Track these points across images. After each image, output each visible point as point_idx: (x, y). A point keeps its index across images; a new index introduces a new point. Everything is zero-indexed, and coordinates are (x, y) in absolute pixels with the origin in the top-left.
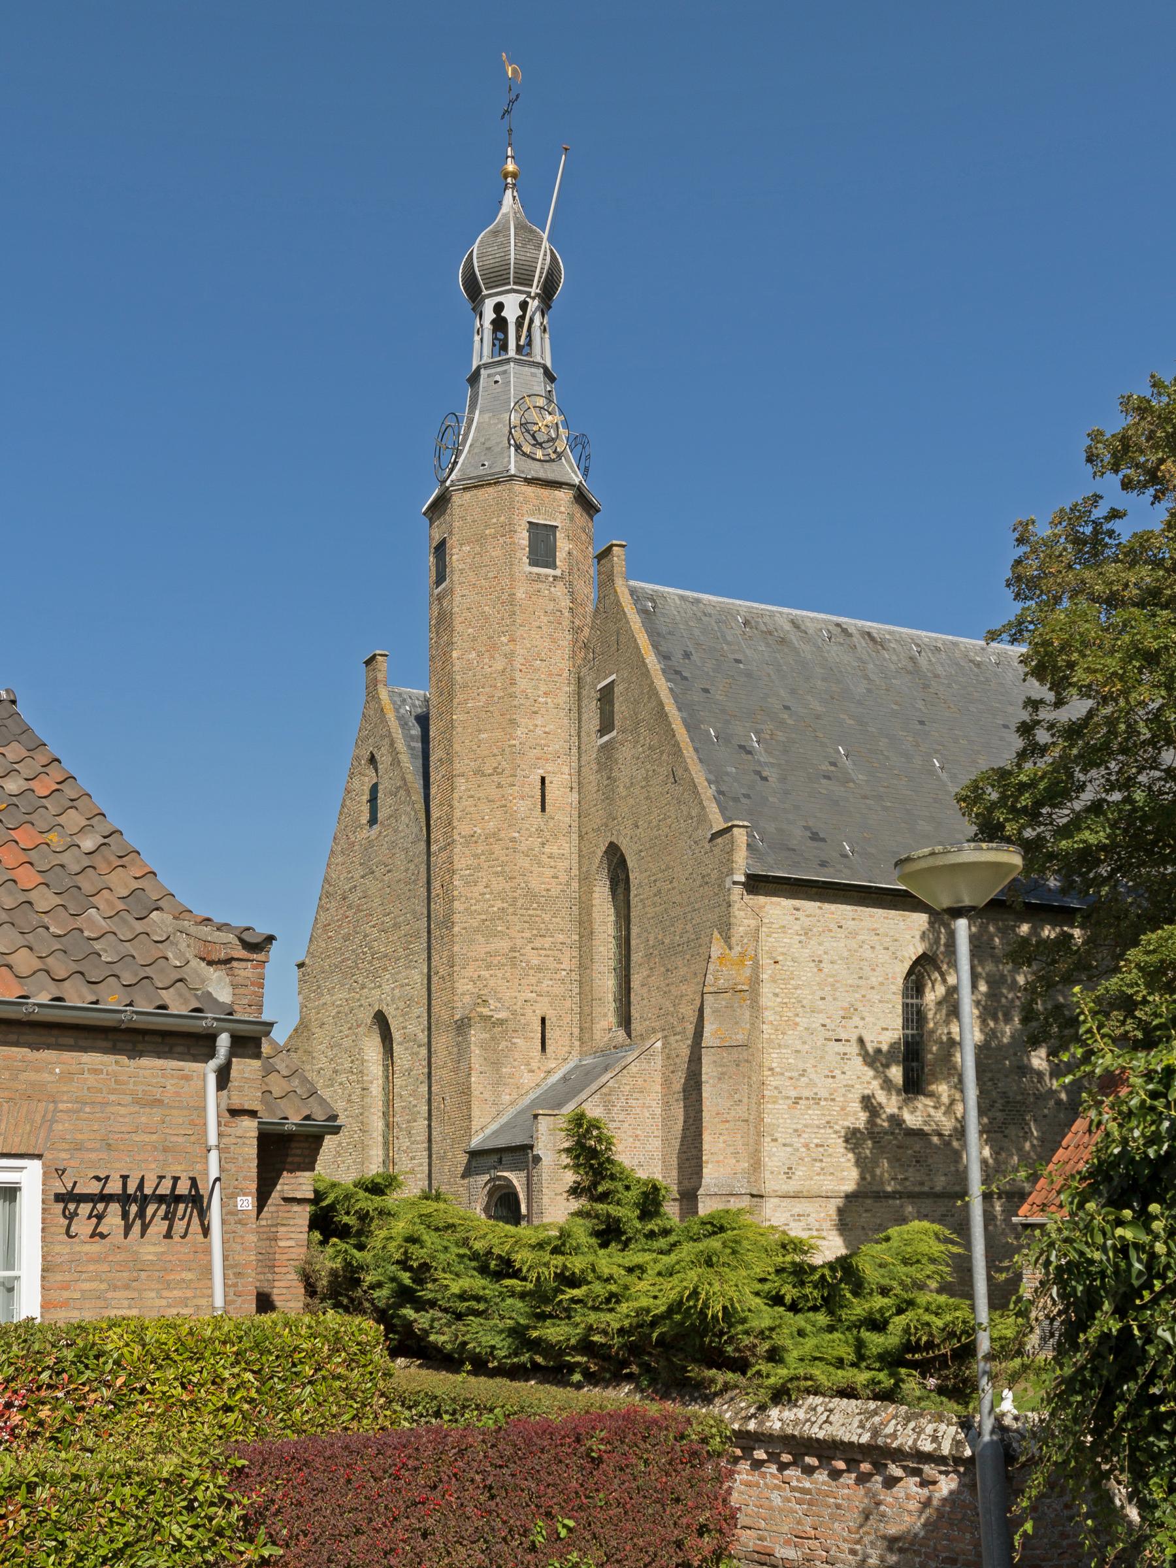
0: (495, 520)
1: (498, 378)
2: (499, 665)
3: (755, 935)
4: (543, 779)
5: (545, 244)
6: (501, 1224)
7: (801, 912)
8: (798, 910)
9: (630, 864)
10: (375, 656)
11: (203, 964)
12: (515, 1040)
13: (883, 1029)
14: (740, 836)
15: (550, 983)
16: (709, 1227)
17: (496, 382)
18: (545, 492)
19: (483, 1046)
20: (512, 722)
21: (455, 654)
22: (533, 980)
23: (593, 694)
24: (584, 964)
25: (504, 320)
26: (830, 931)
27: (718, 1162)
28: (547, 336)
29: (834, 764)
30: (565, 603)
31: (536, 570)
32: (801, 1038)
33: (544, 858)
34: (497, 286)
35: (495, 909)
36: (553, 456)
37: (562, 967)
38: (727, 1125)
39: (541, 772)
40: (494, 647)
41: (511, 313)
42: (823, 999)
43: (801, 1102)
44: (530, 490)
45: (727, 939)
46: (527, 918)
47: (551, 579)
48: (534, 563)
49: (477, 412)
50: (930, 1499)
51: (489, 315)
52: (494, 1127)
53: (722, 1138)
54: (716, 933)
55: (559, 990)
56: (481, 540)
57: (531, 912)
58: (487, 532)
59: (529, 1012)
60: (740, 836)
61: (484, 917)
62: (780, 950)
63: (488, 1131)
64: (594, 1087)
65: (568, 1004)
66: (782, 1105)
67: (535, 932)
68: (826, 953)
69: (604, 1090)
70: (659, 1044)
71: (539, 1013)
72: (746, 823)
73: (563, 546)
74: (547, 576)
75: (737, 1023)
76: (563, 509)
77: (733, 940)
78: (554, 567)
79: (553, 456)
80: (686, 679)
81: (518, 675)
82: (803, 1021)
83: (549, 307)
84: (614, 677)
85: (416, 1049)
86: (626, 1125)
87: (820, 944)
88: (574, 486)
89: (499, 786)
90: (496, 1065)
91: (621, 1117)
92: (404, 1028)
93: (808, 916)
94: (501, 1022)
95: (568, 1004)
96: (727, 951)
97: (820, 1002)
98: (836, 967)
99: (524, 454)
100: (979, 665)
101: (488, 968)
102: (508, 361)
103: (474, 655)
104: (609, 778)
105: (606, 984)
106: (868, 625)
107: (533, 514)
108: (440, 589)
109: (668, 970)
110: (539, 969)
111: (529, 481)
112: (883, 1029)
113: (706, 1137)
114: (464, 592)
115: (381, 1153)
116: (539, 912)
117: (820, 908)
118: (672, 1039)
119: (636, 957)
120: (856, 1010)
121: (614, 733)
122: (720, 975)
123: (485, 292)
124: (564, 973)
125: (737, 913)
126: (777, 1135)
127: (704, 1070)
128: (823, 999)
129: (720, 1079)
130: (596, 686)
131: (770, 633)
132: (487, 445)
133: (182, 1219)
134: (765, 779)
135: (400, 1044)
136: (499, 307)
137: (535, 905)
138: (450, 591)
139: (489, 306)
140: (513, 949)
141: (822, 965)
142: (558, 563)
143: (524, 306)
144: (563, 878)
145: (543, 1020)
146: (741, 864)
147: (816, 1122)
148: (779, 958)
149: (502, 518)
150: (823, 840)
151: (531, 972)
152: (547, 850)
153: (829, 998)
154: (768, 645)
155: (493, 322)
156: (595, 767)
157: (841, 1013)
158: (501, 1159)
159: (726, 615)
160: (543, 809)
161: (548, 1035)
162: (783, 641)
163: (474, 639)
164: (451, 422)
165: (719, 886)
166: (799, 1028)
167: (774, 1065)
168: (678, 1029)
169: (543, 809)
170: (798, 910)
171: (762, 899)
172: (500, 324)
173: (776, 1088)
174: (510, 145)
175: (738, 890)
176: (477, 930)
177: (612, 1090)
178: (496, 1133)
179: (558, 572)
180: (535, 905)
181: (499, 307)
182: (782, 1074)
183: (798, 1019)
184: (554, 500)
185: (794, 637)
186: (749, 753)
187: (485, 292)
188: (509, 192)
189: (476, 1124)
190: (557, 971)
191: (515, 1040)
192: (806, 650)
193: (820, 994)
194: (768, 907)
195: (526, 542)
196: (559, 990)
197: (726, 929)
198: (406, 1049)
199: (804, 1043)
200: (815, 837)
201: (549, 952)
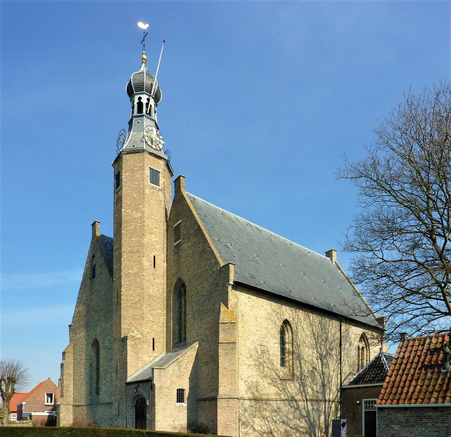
0: (138, 165)
1: (139, 121)
2: (139, 215)
3: (236, 305)
4: (154, 257)
5: (156, 79)
7: (250, 299)
8: (250, 298)
9: (186, 285)
10: (95, 222)
12: (143, 345)
13: (275, 343)
15: (156, 326)
17: (139, 122)
18: (156, 159)
19: (132, 346)
20: (143, 235)
21: (123, 210)
22: (150, 325)
23: (172, 229)
25: (142, 103)
26: (259, 307)
27: (224, 386)
28: (156, 114)
29: (254, 258)
30: (162, 198)
32: (250, 343)
33: (155, 284)
34: (141, 91)
35: (137, 299)
36: (158, 149)
37: (160, 321)
38: (228, 373)
39: (154, 254)
40: (137, 209)
41: (144, 101)
42: (257, 330)
43: (250, 366)
44: (151, 157)
45: (227, 306)
46: (148, 303)
47: (158, 189)
48: (152, 182)
49: (132, 131)
51: (136, 101)
52: (136, 375)
53: (226, 377)
54: (222, 303)
55: (159, 329)
56: (132, 171)
57: (150, 301)
58: (135, 169)
59: (149, 336)
61: (133, 302)
62: (244, 311)
63: (133, 376)
64: (175, 360)
65: (162, 335)
66: (245, 367)
67: (151, 308)
68: (258, 315)
69: (178, 361)
70: (197, 346)
71: (153, 335)
73: (162, 180)
74: (156, 188)
75: (231, 335)
76: (162, 167)
77: (229, 306)
78: (159, 186)
80: (206, 222)
81: (146, 219)
82: (251, 338)
84: (181, 221)
85: (108, 350)
86: (186, 374)
87: (256, 311)
88: (166, 160)
89: (139, 257)
90: (137, 353)
91: (184, 371)
92: (104, 344)
93: (253, 301)
94: (139, 339)
95: (162, 335)
96: (227, 309)
97: (256, 332)
98: (261, 320)
100: (286, 244)
101: (134, 320)
102: (143, 116)
103: (130, 211)
104: (178, 256)
106: (257, 226)
107: (151, 165)
108: (117, 189)
109: (201, 319)
110: (152, 322)
111: (151, 154)
112: (275, 343)
113: (220, 377)
114: (126, 189)
115: (95, 385)
116: (153, 302)
117: (257, 299)
118: (203, 344)
120: (267, 336)
121: (180, 240)
122: (224, 317)
123: (135, 93)
124: (161, 324)
125: (230, 296)
126: (243, 378)
127: (220, 351)
128: (257, 330)
129: (225, 355)
130: (173, 226)
131: (230, 219)
132: (135, 141)
133: (438, 434)
134: (234, 257)
135: (102, 349)
136: (140, 98)
137: (151, 299)
138: (121, 189)
140: (143, 314)
141: (257, 319)
142: (160, 185)
143: (148, 100)
144: (161, 291)
145: (153, 339)
148: (244, 314)
149: (141, 164)
150: (255, 278)
151: (150, 322)
152: (155, 281)
153: (259, 331)
154: (229, 221)
155: (138, 103)
156: (172, 254)
157: (263, 336)
158: (139, 385)
159: (216, 211)
160: (154, 267)
161: (155, 345)
162: (234, 222)
163: (130, 205)
164: (123, 132)
165: (223, 286)
166: (250, 340)
167: (242, 352)
168: (206, 340)
169: (154, 267)
170: (250, 298)
171: (238, 293)
172: (140, 104)
173: (242, 361)
174: (144, 50)
175: (230, 288)
176: (130, 307)
177: (181, 361)
178: (136, 377)
179: (160, 188)
180: (151, 299)
181: (140, 98)
182: (245, 356)
183: (250, 337)
184: (159, 163)
185: (236, 221)
186: (229, 248)
187: (135, 93)
188: (144, 65)
189: (129, 374)
190: (158, 323)
191: (143, 345)
192: (241, 226)
193: (256, 329)
194: (240, 295)
195: (149, 174)
196: (159, 329)
198: (105, 351)
199: (251, 345)
200: (252, 277)
201: (156, 316)
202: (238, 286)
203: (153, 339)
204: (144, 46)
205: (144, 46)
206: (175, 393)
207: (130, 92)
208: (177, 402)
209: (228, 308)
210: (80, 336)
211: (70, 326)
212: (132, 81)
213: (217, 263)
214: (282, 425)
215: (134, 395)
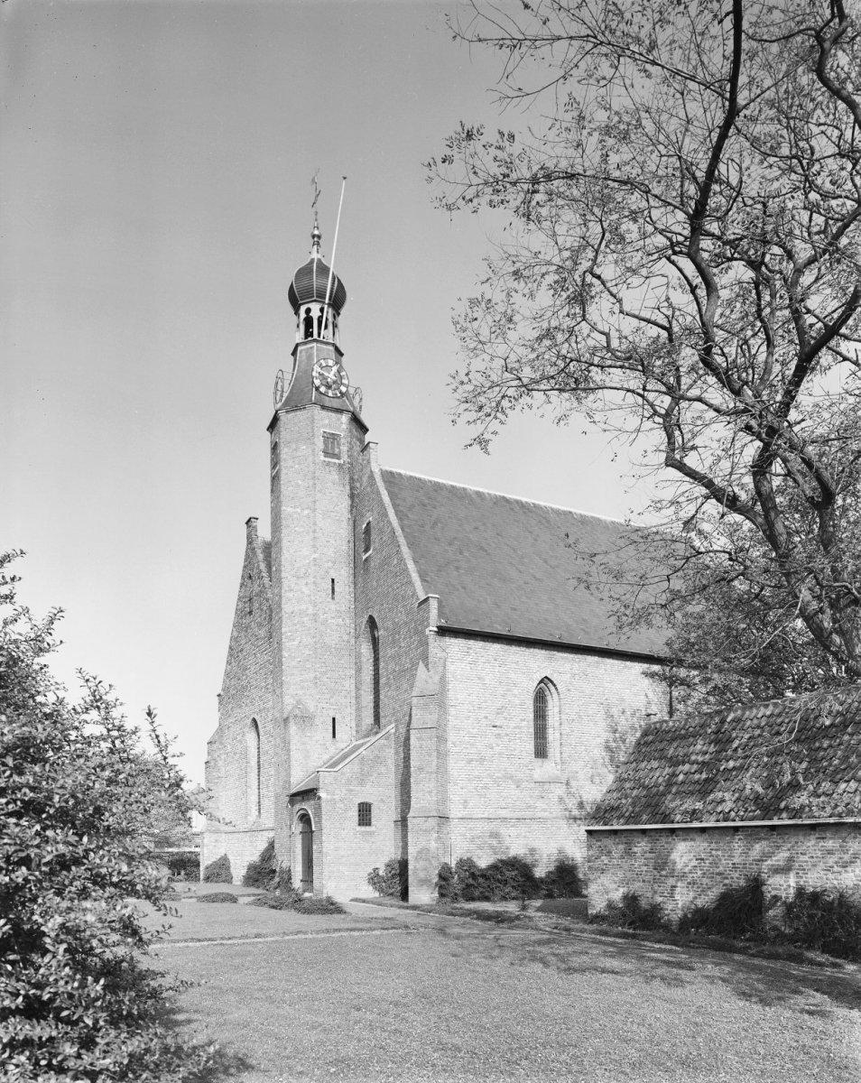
6: (788, 963)
11: (806, 1016)
14: (434, 604)
16: (672, 561)
24: (359, 670)
31: (327, 459)
34: (308, 298)
41: (315, 314)
50: (15, 824)
51: (303, 315)
60: (434, 604)
71: (332, 715)
72: (437, 596)
79: (339, 395)
83: (339, 314)
99: (321, 393)
105: (368, 699)
119: (382, 681)
136: (308, 311)
139: (303, 309)
140: (315, 678)
143: (322, 310)
145: (334, 719)
146: (434, 620)
147: (777, 368)
155: (305, 319)
181: (308, 311)
197: (425, 658)
202: (443, 631)
203: (334, 719)
204: (316, 213)
205: (316, 213)
206: (354, 813)
207: (295, 302)
208: (359, 825)
209: (271, 846)
210: (763, 117)
211: (219, 695)
212: (294, 285)
213: (414, 594)
214: (640, 726)
215: (299, 814)
